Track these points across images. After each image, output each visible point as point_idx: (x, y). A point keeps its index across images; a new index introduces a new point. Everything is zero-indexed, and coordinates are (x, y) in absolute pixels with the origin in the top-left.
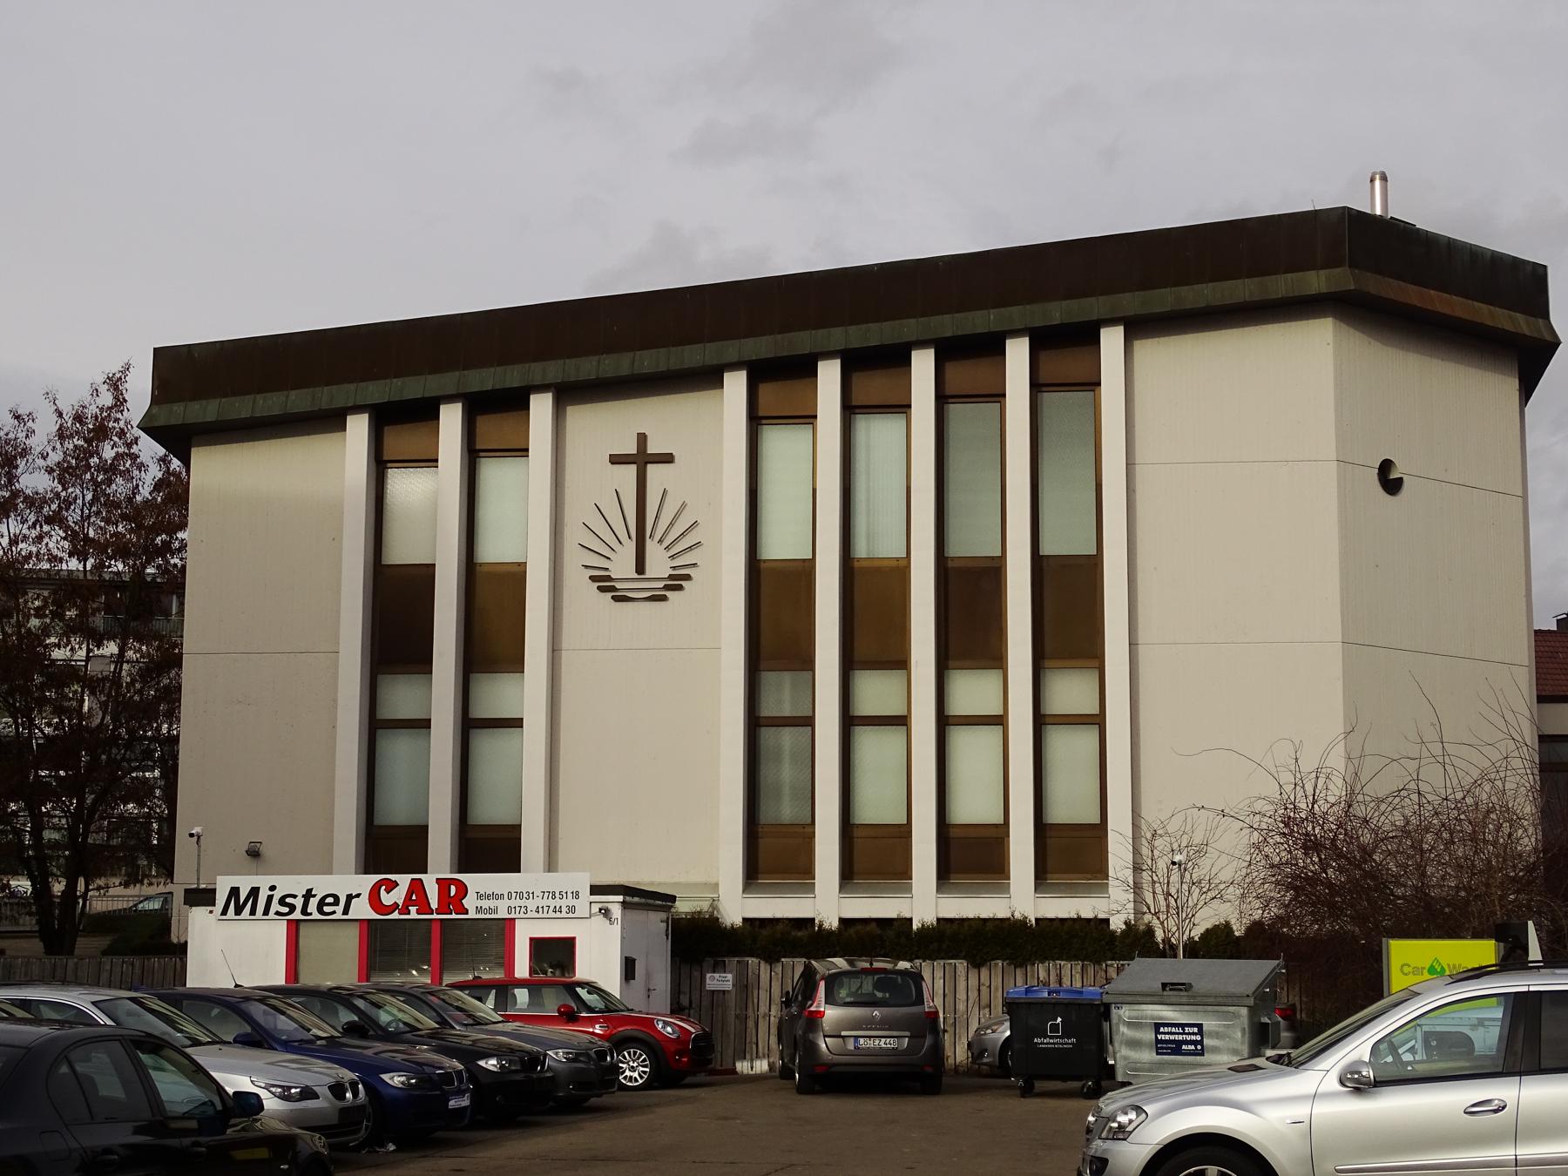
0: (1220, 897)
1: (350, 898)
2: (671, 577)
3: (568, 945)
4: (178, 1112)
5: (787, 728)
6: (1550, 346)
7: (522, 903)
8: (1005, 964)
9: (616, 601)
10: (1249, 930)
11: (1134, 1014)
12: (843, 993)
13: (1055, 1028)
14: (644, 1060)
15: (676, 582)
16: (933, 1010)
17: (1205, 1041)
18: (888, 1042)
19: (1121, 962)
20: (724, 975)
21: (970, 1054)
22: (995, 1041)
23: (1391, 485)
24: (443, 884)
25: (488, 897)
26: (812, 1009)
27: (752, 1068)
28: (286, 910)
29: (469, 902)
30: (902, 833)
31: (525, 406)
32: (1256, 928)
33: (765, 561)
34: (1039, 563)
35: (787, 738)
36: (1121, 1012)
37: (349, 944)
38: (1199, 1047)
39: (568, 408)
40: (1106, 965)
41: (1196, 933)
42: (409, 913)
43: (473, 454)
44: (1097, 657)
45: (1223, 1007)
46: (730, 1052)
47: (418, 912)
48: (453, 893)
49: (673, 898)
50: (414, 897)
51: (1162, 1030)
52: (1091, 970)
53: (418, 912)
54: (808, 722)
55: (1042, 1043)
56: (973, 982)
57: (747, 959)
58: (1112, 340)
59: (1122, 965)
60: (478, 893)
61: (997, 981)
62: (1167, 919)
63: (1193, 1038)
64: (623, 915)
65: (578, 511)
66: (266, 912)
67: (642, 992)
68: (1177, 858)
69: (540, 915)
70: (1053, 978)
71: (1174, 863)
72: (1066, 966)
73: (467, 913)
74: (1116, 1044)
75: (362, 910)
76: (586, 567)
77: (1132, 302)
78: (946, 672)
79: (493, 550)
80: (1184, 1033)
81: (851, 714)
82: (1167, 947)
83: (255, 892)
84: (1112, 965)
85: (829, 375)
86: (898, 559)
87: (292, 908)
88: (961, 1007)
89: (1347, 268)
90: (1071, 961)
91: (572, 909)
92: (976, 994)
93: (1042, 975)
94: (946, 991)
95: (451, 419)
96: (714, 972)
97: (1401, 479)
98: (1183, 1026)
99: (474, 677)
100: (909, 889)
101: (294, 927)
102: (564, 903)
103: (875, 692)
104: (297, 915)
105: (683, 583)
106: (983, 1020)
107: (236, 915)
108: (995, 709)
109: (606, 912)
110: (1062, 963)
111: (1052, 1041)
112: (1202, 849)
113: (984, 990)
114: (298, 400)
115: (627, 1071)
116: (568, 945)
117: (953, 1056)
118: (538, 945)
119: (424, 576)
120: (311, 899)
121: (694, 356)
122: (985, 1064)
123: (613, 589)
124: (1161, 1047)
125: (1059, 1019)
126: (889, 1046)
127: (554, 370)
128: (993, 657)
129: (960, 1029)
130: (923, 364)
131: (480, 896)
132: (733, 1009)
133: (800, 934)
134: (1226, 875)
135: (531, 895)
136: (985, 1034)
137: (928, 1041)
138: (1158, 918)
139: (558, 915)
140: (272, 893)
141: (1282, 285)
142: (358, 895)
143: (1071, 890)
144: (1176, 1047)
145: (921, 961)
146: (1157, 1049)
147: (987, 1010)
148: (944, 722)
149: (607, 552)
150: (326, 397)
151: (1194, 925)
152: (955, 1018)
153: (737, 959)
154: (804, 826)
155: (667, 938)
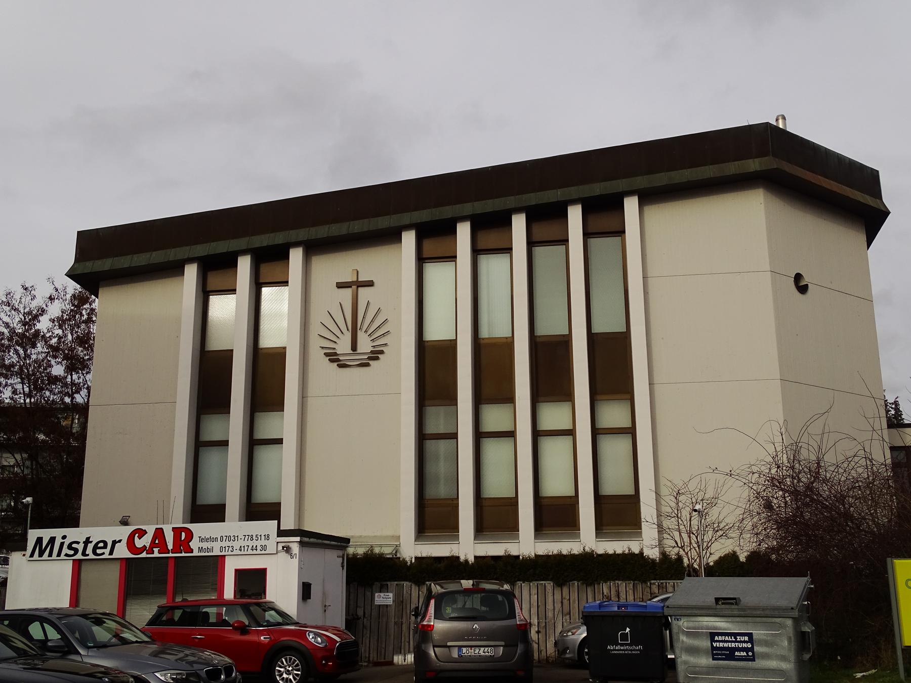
0: (725, 535)
1: (114, 543)
2: (372, 352)
3: (261, 574)
5: (442, 440)
6: (882, 214)
7: (230, 544)
8: (579, 584)
9: (339, 367)
10: (748, 558)
11: (691, 624)
12: (449, 610)
13: (624, 637)
14: (297, 665)
15: (375, 355)
16: (524, 623)
17: (756, 649)
18: (486, 650)
19: (661, 581)
20: (388, 594)
21: (556, 650)
22: (575, 640)
23: (803, 289)
24: (177, 531)
25: (207, 540)
26: (425, 623)
27: (405, 660)
28: (72, 552)
29: (194, 544)
30: (512, 503)
31: (287, 257)
32: (754, 556)
33: (428, 341)
34: (592, 338)
35: (443, 446)
36: (681, 623)
37: (113, 575)
38: (750, 654)
39: (313, 257)
40: (651, 584)
41: (711, 561)
42: (153, 553)
43: (257, 285)
44: (629, 393)
45: (770, 619)
46: (391, 648)
47: (160, 552)
48: (183, 538)
49: (347, 541)
50: (157, 542)
51: (716, 638)
52: (639, 587)
53: (160, 552)
54: (454, 436)
55: (614, 650)
56: (558, 596)
57: (402, 583)
58: (631, 205)
59: (662, 583)
60: (200, 537)
61: (574, 596)
62: (690, 550)
63: (745, 645)
64: (301, 552)
65: (318, 316)
66: (59, 555)
67: (320, 609)
68: (697, 507)
69: (242, 552)
70: (613, 592)
71: (695, 511)
72: (622, 585)
73: (192, 552)
74: (677, 651)
75: (122, 552)
76: (322, 348)
77: (642, 182)
78: (537, 404)
79: (268, 341)
80: (736, 641)
81: (480, 431)
82: (691, 570)
83: (52, 540)
84: (654, 584)
85: (464, 231)
86: (507, 338)
87: (76, 551)
88: (550, 614)
89: (771, 156)
90: (626, 581)
91: (264, 548)
92: (560, 605)
93: (606, 591)
94: (539, 604)
95: (244, 264)
96: (380, 592)
97: (807, 285)
98: (735, 635)
99: (257, 414)
100: (517, 537)
101: (78, 564)
102: (259, 543)
103: (495, 418)
104: (79, 556)
105: (379, 356)
106: (565, 624)
107: (39, 557)
108: (568, 426)
109: (287, 549)
110: (620, 582)
111: (622, 648)
112: (712, 504)
113: (566, 602)
114: (157, 257)
115: (284, 674)
116: (261, 574)
117: (545, 650)
118: (239, 573)
119: (227, 356)
120: (89, 544)
121: (383, 222)
122: (567, 659)
124: (716, 653)
125: (628, 630)
126: (487, 654)
127: (303, 234)
128: (566, 394)
129: (549, 630)
130: (519, 223)
131: (202, 540)
132: (393, 618)
133: (439, 566)
134: (730, 520)
135: (236, 538)
136: (567, 636)
137: (520, 649)
138: (684, 550)
139: (255, 552)
140: (63, 541)
141: (732, 168)
142: (120, 541)
143: (619, 536)
144: (730, 654)
145: (521, 582)
146: (713, 655)
147: (568, 616)
148: (537, 434)
149: (334, 339)
150: (173, 254)
151: (711, 554)
152: (546, 623)
153: (396, 583)
154: (452, 500)
155: (343, 569)
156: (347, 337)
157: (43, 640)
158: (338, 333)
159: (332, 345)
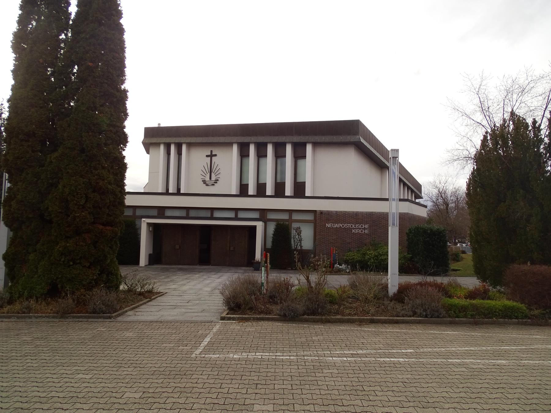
4: (8, 230)
105: (217, 182)
123: (206, 183)
141: (341, 138)
149: (205, 175)
156: (208, 175)
157: (291, 247)
158: (208, 172)
159: (204, 178)
